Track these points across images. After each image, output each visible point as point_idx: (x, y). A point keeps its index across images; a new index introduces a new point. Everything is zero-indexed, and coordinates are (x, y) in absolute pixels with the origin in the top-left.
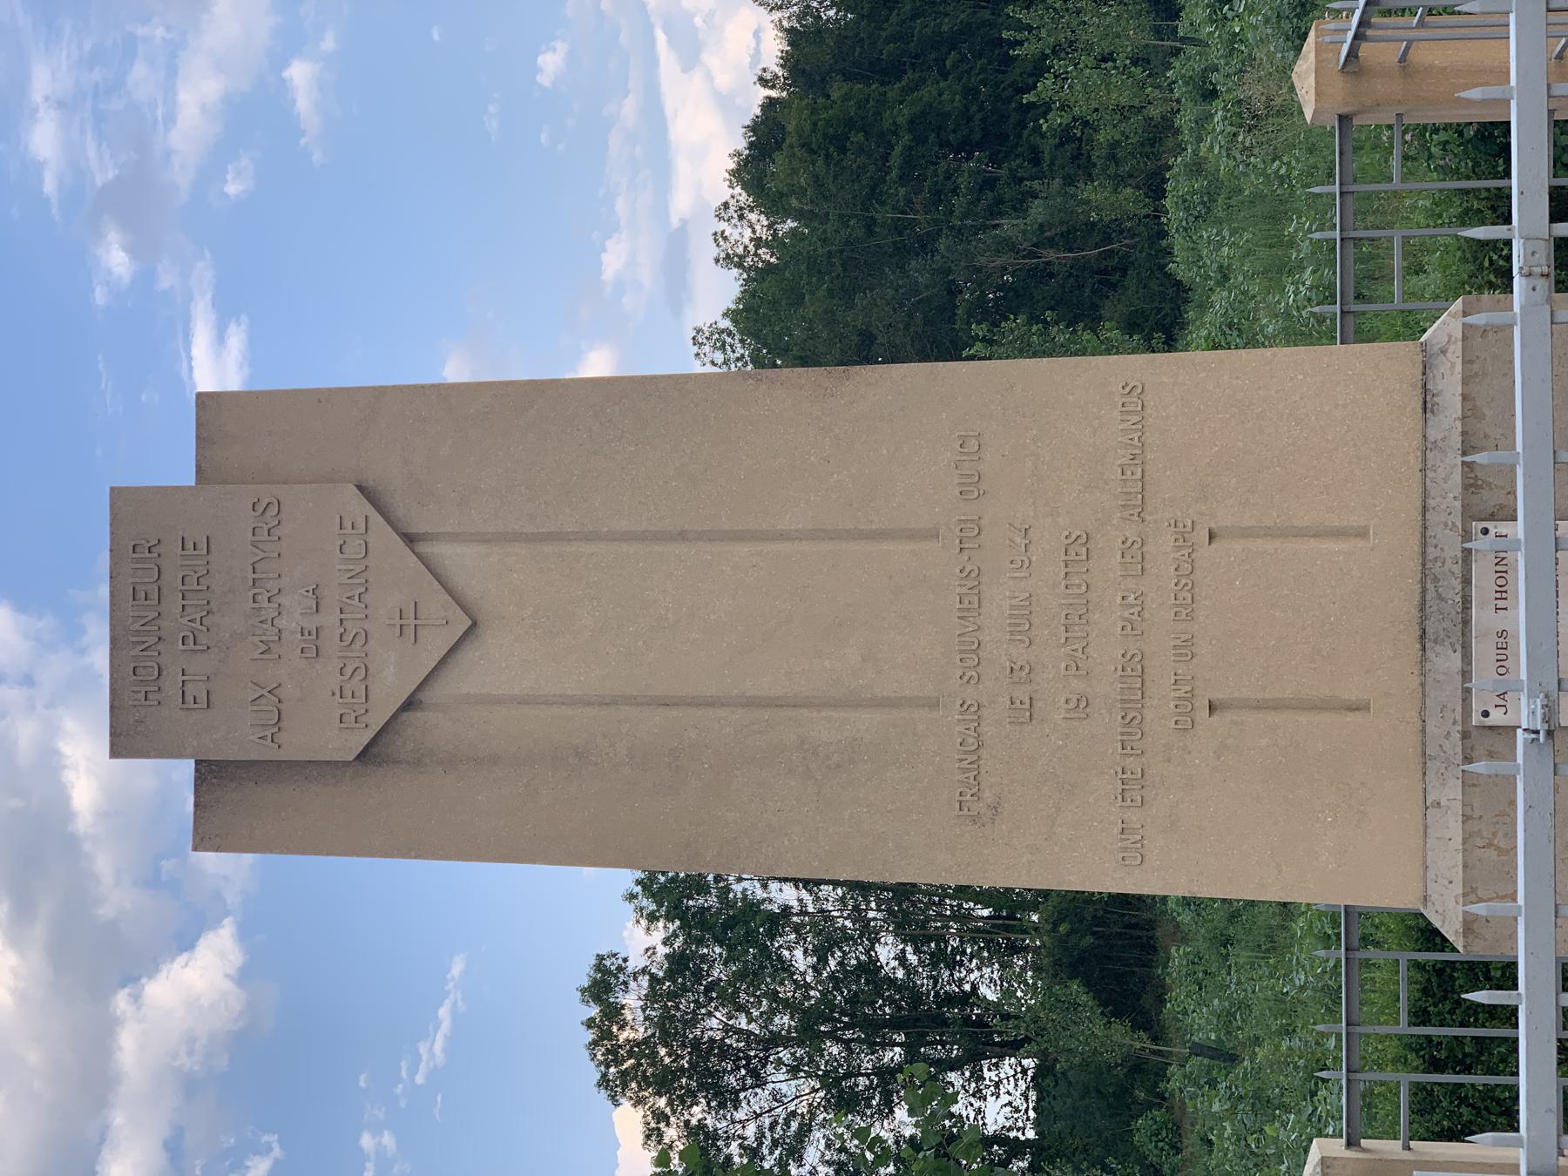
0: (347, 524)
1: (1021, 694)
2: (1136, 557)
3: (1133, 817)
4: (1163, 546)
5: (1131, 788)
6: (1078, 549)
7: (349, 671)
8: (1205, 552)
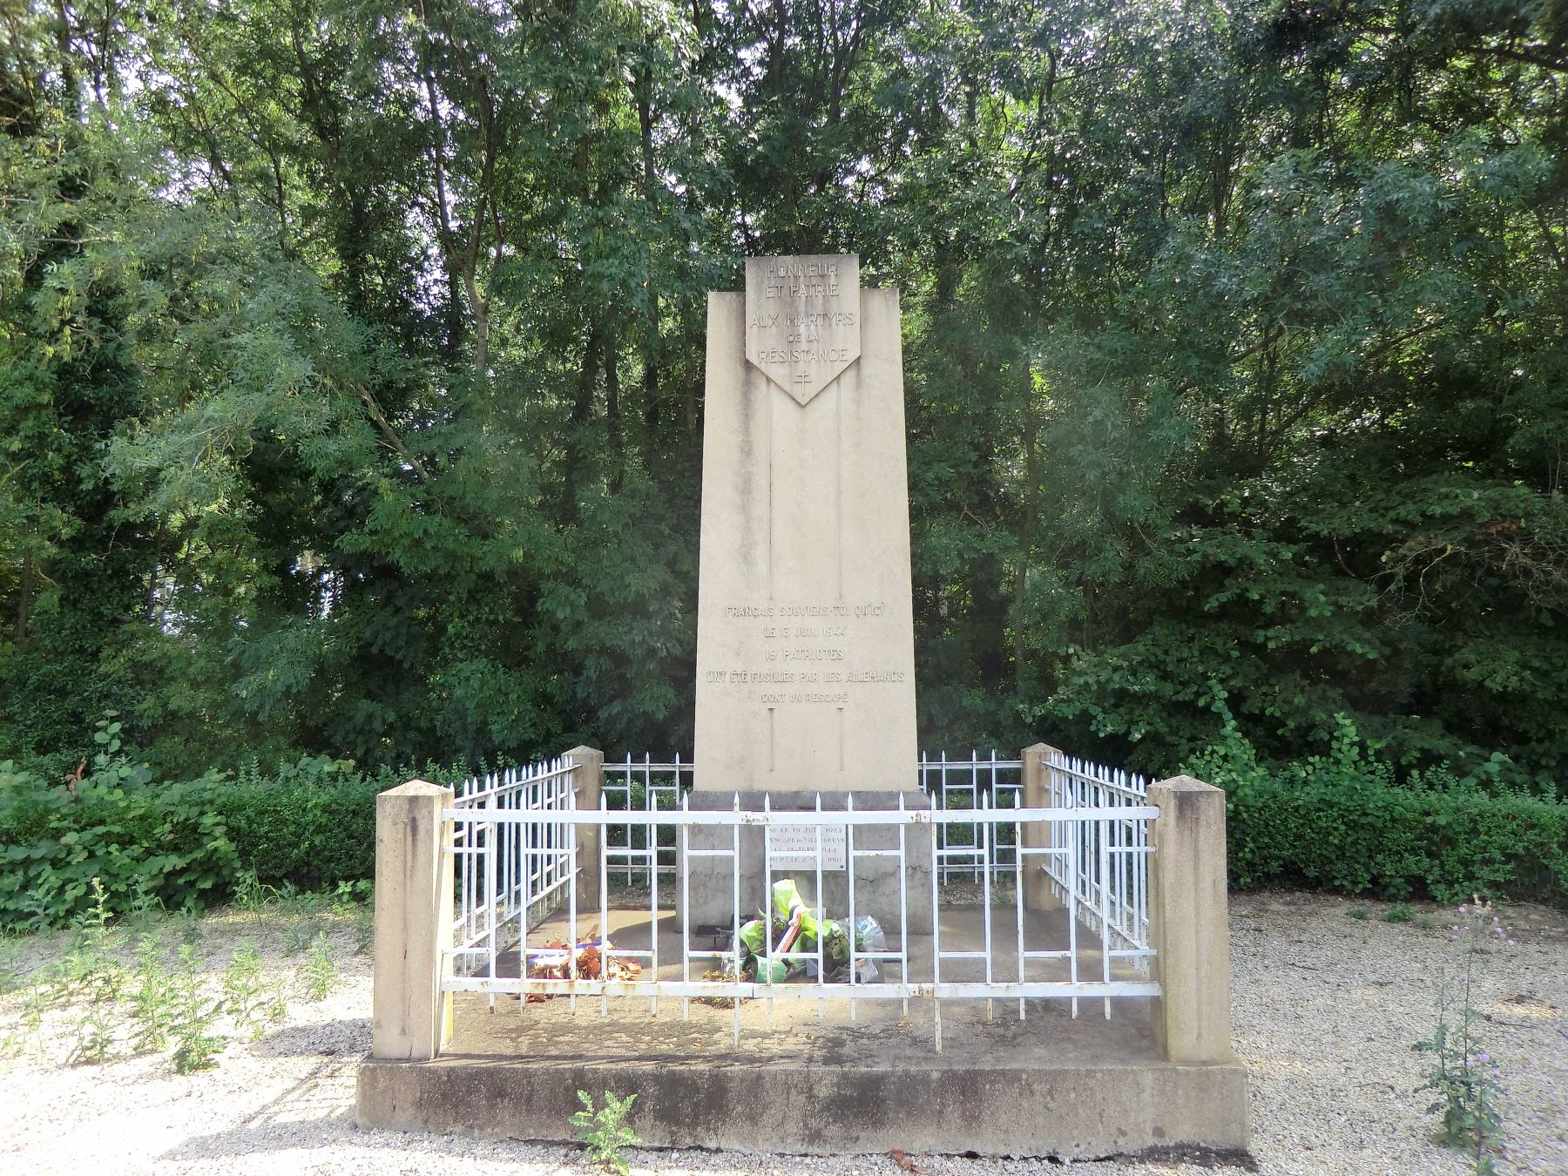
1: (777, 632)
2: (833, 678)
3: (728, 677)
5: (742, 676)
6: (836, 656)
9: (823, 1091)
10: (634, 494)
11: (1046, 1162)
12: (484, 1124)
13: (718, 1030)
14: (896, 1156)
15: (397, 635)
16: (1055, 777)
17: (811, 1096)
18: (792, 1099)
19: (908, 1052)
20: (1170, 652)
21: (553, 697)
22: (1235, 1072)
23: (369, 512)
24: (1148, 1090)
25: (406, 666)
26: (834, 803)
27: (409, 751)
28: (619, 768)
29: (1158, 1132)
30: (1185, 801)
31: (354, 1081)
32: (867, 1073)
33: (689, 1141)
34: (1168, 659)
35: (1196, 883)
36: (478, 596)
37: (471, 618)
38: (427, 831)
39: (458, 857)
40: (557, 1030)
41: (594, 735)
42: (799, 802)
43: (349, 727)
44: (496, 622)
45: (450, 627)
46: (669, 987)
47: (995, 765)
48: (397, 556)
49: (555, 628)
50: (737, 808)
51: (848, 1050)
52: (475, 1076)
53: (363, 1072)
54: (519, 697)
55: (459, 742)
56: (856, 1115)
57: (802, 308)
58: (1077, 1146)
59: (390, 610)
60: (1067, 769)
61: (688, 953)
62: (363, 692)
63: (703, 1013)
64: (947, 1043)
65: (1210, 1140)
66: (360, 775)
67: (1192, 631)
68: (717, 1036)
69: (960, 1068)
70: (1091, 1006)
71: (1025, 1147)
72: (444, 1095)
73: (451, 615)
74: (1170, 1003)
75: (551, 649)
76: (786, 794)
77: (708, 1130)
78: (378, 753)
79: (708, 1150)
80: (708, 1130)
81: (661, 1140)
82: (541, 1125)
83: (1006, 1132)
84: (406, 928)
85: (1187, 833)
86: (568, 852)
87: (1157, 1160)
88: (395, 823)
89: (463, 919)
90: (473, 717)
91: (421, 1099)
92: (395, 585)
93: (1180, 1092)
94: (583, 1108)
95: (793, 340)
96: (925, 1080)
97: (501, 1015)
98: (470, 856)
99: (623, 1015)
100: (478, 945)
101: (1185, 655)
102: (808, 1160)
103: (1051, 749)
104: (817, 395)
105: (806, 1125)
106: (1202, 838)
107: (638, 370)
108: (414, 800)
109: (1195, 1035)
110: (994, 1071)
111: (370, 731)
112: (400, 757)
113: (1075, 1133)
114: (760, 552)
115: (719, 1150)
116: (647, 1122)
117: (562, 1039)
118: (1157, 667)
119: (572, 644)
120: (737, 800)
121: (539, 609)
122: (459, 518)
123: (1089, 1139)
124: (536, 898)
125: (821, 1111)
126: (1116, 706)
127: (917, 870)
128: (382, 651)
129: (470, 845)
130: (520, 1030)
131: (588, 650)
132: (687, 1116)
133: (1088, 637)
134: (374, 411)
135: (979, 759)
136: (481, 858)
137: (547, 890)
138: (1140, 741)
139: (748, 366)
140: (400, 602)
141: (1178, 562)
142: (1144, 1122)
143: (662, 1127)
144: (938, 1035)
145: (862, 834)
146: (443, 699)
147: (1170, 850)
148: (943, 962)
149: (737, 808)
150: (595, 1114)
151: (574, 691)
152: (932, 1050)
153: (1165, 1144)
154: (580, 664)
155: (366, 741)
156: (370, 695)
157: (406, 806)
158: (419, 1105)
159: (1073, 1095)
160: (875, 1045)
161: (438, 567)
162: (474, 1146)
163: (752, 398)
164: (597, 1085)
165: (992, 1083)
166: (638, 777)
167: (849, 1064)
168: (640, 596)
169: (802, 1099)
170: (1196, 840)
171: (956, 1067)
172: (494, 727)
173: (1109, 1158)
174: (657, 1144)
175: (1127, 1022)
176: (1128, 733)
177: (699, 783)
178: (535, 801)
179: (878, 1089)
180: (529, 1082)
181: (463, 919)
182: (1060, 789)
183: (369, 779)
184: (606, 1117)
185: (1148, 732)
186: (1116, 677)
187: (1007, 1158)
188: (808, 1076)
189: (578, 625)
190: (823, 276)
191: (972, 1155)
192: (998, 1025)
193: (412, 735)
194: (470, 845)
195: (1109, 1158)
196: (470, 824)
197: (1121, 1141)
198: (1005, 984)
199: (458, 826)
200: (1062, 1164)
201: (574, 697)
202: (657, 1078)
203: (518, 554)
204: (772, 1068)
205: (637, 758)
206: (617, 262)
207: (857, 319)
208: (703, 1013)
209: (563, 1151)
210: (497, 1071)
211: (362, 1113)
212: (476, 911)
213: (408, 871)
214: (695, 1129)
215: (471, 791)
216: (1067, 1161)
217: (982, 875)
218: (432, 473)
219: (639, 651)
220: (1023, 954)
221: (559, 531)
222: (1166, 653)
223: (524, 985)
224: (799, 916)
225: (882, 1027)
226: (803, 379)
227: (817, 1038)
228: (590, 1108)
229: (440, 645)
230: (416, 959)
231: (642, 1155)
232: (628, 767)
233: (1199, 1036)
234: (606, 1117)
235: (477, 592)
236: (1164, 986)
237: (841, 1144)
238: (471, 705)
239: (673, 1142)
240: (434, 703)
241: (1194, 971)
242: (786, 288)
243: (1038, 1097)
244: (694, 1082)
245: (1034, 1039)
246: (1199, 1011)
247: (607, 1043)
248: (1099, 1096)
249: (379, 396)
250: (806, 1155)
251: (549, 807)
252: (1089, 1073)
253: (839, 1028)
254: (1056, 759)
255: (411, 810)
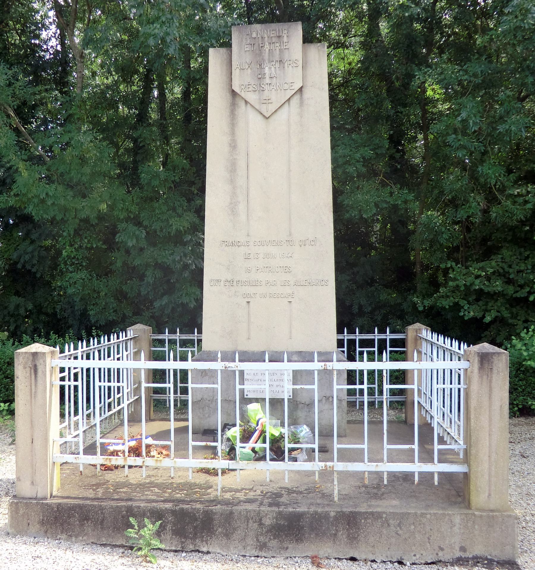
0: (292, 84)
2: (285, 284)
3: (222, 283)
4: (288, 290)
5: (230, 283)
6: (287, 270)
7: (254, 86)
8: (286, 301)
9: (267, 522)
10: (174, 168)
11: (396, 564)
12: (78, 535)
13: (211, 487)
14: (315, 561)
15: (33, 257)
16: (424, 344)
17: (261, 524)
18: (250, 525)
19: (319, 501)
20: (513, 266)
21: (127, 294)
22: (510, 516)
23: (14, 182)
24: (458, 525)
25: (38, 275)
26: (276, 358)
27: (41, 327)
28: (161, 337)
29: (463, 549)
30: (484, 358)
31: (7, 512)
32: (293, 512)
33: (191, 547)
34: (511, 270)
35: (490, 406)
36: (81, 233)
37: (76, 246)
38: (43, 372)
39: (62, 388)
40: (118, 486)
41: (152, 317)
42: (258, 357)
43: (6, 312)
44: (92, 248)
45: (64, 252)
46: (181, 462)
47: (389, 336)
48: (30, 209)
49: (128, 252)
50: (219, 360)
51: (284, 499)
52: (73, 508)
53: (11, 504)
54: (106, 294)
55: (70, 322)
56: (286, 536)
57: (266, 56)
58: (415, 555)
59: (28, 242)
60: (430, 339)
61: (191, 443)
62: (14, 291)
63: (202, 478)
64: (342, 497)
65: (493, 554)
66: (12, 341)
67: (528, 253)
68: (209, 491)
69: (346, 510)
70: (426, 477)
71: (384, 555)
72: (56, 518)
73: (64, 244)
74: (472, 476)
75: (125, 264)
76: (257, 353)
77: (202, 541)
78: (23, 329)
79: (202, 552)
80: (202, 541)
81: (176, 546)
82: (109, 536)
83: (373, 546)
84: (32, 426)
85: (485, 377)
86: (126, 386)
87: (461, 565)
88: (25, 368)
89: (66, 423)
90: (78, 307)
91: (43, 520)
92: (30, 226)
93: (476, 527)
94: (132, 527)
95: (261, 77)
96: (326, 516)
97: (88, 477)
98: (69, 386)
99: (157, 478)
100: (75, 437)
101: (522, 268)
102: (259, 560)
103: (424, 327)
104: (276, 111)
105: (258, 540)
106: (494, 380)
107: (178, 90)
108: (35, 355)
109: (487, 494)
110: (367, 513)
111: (19, 315)
112: (36, 331)
113: (414, 548)
114: (242, 207)
115: (208, 553)
116: (168, 536)
117: (121, 490)
118: (504, 276)
119: (137, 262)
120: (219, 355)
121: (117, 240)
122: (68, 185)
123: (422, 552)
124: (111, 413)
125: (267, 532)
126: (477, 300)
127: (327, 399)
128: (24, 266)
129: (104, 382)
130: (98, 485)
131: (147, 265)
132: (190, 533)
133: (462, 257)
134: (16, 121)
135: (379, 332)
136: (76, 387)
137: (118, 408)
138: (492, 322)
139: (234, 94)
140: (33, 237)
141: (517, 209)
142: (455, 543)
143: (176, 539)
144: (336, 492)
145: (297, 376)
146: (61, 295)
147: (475, 387)
148: (339, 450)
149: (219, 360)
150: (139, 531)
151: (139, 290)
152: (332, 500)
153: (467, 556)
154: (144, 273)
155: (16, 321)
156: (17, 294)
157: (31, 358)
158: (42, 523)
159: (413, 527)
160: (300, 497)
161: (55, 215)
162: (72, 546)
163: (236, 113)
164: (140, 515)
165: (365, 519)
166: (172, 342)
167: (283, 507)
168: (178, 232)
169: (256, 525)
170: (491, 382)
171: (344, 510)
172: (91, 313)
173: (433, 563)
174: (174, 548)
175: (451, 488)
176: (484, 317)
177: (206, 346)
178: (109, 356)
179: (299, 521)
180: (102, 513)
181: (66, 423)
182: (427, 351)
183: (16, 343)
184: (145, 532)
185: (496, 317)
186: (477, 282)
187: (373, 561)
188: (259, 513)
189: (141, 249)
190: (279, 37)
191: (353, 559)
192: (374, 488)
193: (43, 317)
194: (104, 382)
195: (433, 563)
196: (69, 368)
197: (441, 554)
198: (376, 464)
199: (62, 370)
200: (405, 565)
201: (139, 294)
202: (173, 512)
203: (104, 207)
204: (239, 508)
205: (173, 331)
206: (158, 26)
207: (300, 63)
208: (202, 478)
209: (121, 550)
210: (84, 506)
211: (11, 526)
212: (73, 419)
213: (33, 395)
214: (195, 540)
215: (69, 349)
216: (408, 564)
217: (381, 403)
218: (51, 158)
219: (178, 266)
220: (386, 446)
221: (129, 192)
222: (510, 267)
223: (98, 459)
224: (262, 425)
225: (306, 487)
226: (267, 101)
227: (267, 493)
228: (136, 527)
229: (58, 263)
230: (38, 443)
231: (165, 554)
232: (166, 336)
233: (490, 495)
234: (145, 532)
235: (81, 230)
236: (469, 466)
237: (278, 551)
238: (77, 299)
239: (182, 547)
240: (56, 298)
241: (487, 458)
242: (256, 45)
243: (392, 527)
244: (194, 515)
245: (393, 496)
246: (490, 481)
247: (146, 493)
248: (428, 528)
249: (18, 112)
250: (258, 557)
251: (118, 359)
252: (423, 515)
253: (281, 488)
254: (426, 333)
255: (34, 360)
